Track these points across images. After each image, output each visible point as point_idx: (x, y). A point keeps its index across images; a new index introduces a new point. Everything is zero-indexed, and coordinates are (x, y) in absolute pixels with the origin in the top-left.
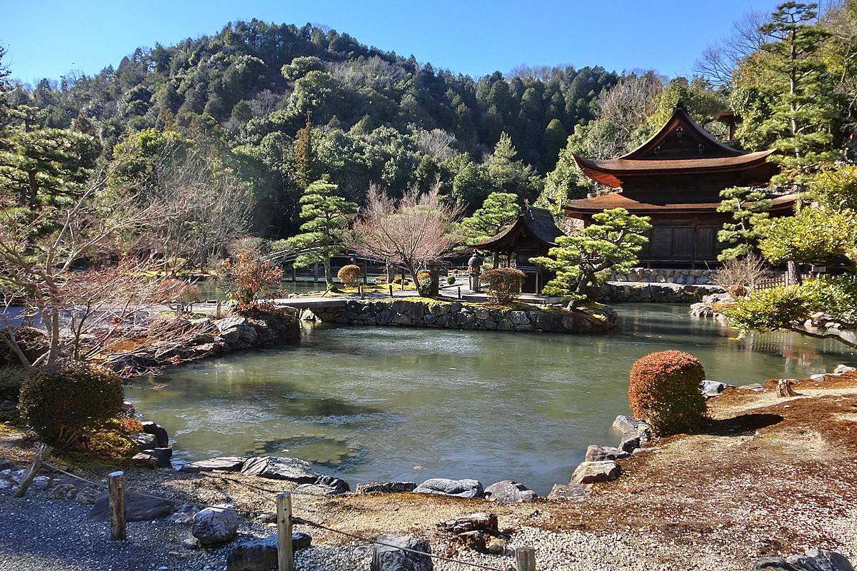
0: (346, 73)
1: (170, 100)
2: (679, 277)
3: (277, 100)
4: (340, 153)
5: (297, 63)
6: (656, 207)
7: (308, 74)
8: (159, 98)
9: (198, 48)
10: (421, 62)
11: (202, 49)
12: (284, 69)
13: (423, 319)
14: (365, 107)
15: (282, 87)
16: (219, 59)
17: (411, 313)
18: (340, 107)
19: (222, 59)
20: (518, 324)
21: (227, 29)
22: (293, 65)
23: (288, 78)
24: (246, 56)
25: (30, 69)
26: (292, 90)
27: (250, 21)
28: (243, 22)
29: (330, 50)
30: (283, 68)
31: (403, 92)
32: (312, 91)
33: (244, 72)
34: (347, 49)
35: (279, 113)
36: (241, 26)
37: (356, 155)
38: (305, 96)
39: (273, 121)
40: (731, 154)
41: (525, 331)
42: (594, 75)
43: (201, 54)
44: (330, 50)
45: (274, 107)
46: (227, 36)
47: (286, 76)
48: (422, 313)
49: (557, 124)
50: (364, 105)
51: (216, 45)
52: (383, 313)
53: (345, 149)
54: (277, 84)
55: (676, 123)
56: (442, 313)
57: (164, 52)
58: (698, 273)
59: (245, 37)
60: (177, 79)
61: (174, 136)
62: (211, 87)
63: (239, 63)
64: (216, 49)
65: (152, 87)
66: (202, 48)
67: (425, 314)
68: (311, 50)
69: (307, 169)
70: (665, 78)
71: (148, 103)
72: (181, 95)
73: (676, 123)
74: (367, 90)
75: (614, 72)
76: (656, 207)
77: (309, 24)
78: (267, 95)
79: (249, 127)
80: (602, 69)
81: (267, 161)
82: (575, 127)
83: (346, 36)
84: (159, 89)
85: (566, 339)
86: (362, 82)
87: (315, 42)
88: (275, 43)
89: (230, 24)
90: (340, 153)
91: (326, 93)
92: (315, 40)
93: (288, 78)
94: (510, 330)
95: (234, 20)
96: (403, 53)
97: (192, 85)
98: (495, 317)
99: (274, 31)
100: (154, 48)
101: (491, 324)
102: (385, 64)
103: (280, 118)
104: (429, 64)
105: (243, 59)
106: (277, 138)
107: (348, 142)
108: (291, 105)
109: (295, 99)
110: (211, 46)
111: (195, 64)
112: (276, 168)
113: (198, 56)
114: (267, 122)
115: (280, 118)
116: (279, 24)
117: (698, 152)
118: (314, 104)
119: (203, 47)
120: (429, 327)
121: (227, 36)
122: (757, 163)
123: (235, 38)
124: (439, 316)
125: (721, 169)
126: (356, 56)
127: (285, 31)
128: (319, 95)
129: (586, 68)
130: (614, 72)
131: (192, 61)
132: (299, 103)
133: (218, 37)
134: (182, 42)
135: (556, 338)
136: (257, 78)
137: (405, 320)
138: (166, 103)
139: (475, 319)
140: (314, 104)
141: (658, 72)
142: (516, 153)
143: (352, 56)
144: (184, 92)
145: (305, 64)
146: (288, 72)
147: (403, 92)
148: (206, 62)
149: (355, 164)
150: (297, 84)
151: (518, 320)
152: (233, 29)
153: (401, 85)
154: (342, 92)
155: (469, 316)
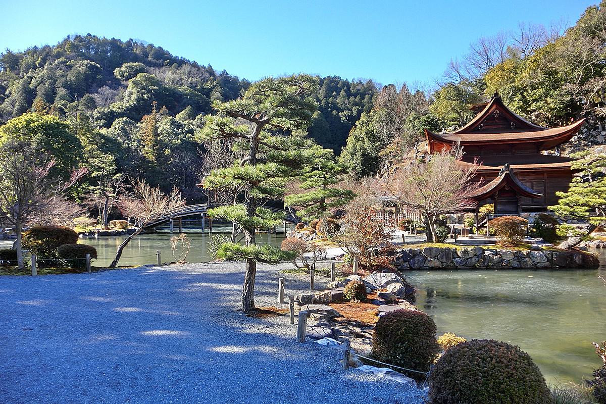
0: (167, 76)
1: (25, 93)
2: (94, 213)
3: (114, 95)
4: (176, 134)
5: (127, 67)
6: (494, 168)
7: (138, 76)
8: (15, 91)
9: (44, 54)
10: (218, 69)
11: (48, 55)
12: (116, 72)
13: (452, 262)
14: (186, 100)
15: (116, 84)
16: (62, 63)
17: (442, 257)
18: (170, 101)
19: (65, 62)
20: (538, 263)
21: (67, 40)
22: (123, 69)
23: (120, 78)
24: (86, 61)
25: (19, 41)
26: (127, 87)
27: (86, 35)
28: (80, 36)
29: (150, 59)
30: (116, 71)
31: (210, 90)
32: (143, 88)
33: (85, 73)
34: (162, 58)
35: (118, 104)
36: (78, 37)
37: (189, 135)
38: (138, 92)
39: (114, 110)
40: (534, 129)
41: (545, 268)
42: (334, 81)
43: (48, 58)
44: (150, 59)
45: (112, 99)
46: (67, 46)
47: (119, 77)
48: (452, 256)
49: (319, 115)
50: (184, 99)
51: (59, 52)
52: (416, 258)
53: (180, 131)
54: (112, 83)
55: (494, 107)
56: (470, 256)
57: (13, 56)
58: (527, 215)
59: (80, 46)
60: (28, 77)
61: (54, 119)
62: (59, 82)
63: (81, 66)
64: (59, 55)
65: (5, 82)
66: (45, 55)
67: (454, 258)
68: (135, 59)
69: (154, 146)
70: (380, 84)
71: (4, 95)
72: (33, 89)
73: (494, 107)
74: (184, 89)
75: (347, 80)
76: (494, 168)
77: (131, 39)
78: (106, 90)
79: (95, 114)
80: (339, 77)
81: (120, 140)
82: (362, 114)
83: (161, 48)
84: (13, 84)
85: (530, 272)
86: (180, 82)
87: (138, 52)
88: (106, 52)
89: (69, 37)
90: (176, 134)
91: (154, 90)
92: (138, 51)
93: (120, 78)
94: (532, 268)
95: (72, 33)
96: (202, 62)
97: (42, 82)
98: (518, 257)
99: (105, 42)
100: (5, 53)
101: (515, 264)
102: (194, 70)
103: (119, 108)
104: (225, 70)
105: (83, 63)
106: (125, 122)
107: (179, 126)
108: (127, 98)
109: (130, 95)
110: (54, 52)
111: (42, 66)
112: (127, 145)
113: (44, 60)
114: (109, 110)
115: (119, 108)
116: (109, 38)
117: (511, 128)
118: (146, 97)
119: (48, 53)
120: (460, 269)
121: (67, 46)
122: (565, 134)
123: (74, 47)
124: (467, 259)
125: (534, 140)
126: (171, 64)
127: (115, 43)
128: (149, 91)
129: (328, 77)
130: (347, 80)
131: (38, 63)
132: (134, 97)
133: (60, 46)
134: (28, 50)
135: (586, 272)
136: (96, 78)
137: (436, 263)
138: (21, 95)
139: (501, 260)
140: (146, 97)
141: (376, 80)
142: (307, 133)
143: (168, 63)
144: (36, 88)
145: (133, 69)
146: (120, 74)
147: (210, 90)
148: (52, 64)
149: (188, 142)
150: (130, 82)
151: (539, 259)
152: (72, 40)
153: (208, 85)
154: (166, 89)
155: (495, 257)
